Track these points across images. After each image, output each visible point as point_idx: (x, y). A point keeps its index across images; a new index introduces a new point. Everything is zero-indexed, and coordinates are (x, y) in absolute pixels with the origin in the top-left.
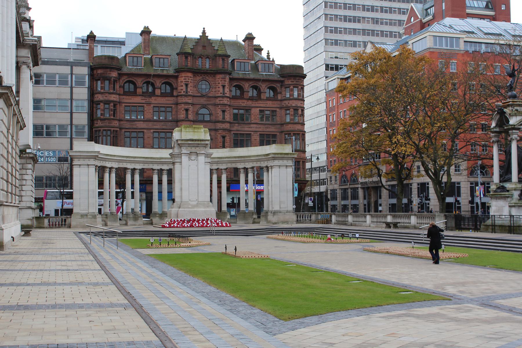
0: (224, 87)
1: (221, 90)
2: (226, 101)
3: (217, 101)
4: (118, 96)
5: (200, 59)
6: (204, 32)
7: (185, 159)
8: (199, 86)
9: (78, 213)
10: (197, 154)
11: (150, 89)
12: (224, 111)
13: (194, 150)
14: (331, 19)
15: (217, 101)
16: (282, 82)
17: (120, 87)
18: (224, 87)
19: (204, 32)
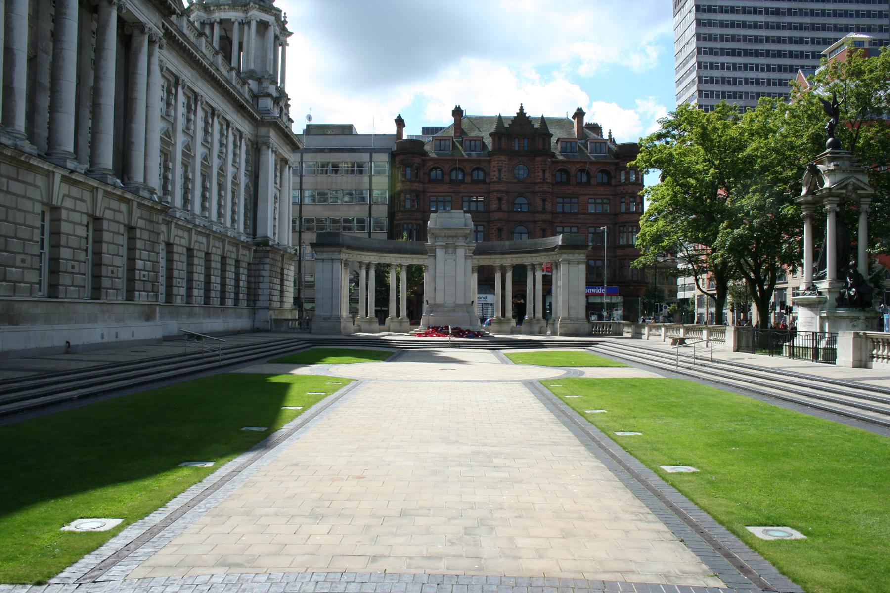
0: (544, 171)
1: (541, 174)
2: (546, 188)
3: (537, 188)
4: (421, 185)
5: (517, 140)
6: (521, 109)
7: (440, 253)
8: (516, 172)
9: (320, 316)
10: (456, 247)
11: (460, 177)
12: (544, 200)
13: (450, 241)
14: (706, 96)
15: (537, 188)
16: (617, 164)
17: (425, 174)
18: (544, 171)
19: (521, 109)
